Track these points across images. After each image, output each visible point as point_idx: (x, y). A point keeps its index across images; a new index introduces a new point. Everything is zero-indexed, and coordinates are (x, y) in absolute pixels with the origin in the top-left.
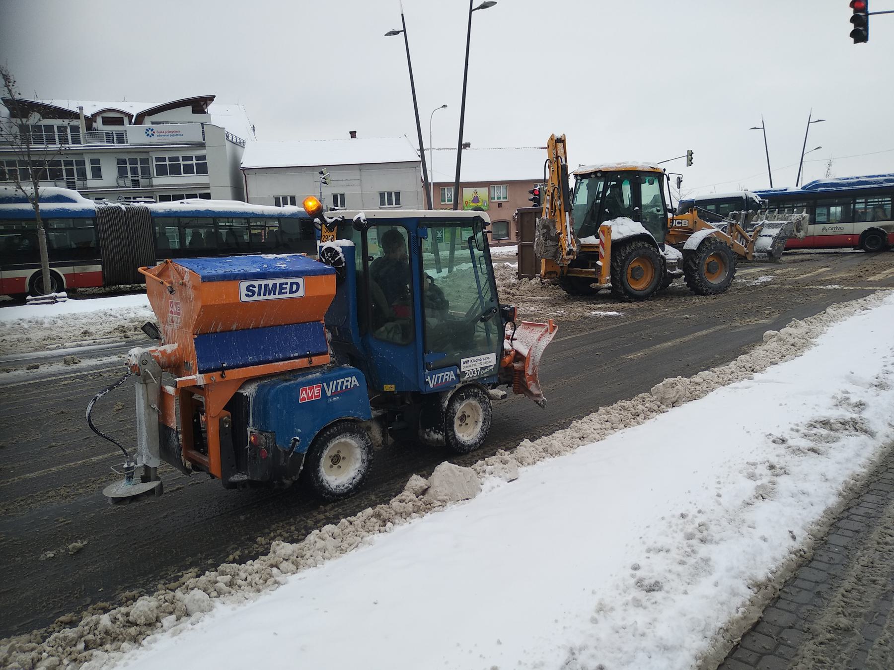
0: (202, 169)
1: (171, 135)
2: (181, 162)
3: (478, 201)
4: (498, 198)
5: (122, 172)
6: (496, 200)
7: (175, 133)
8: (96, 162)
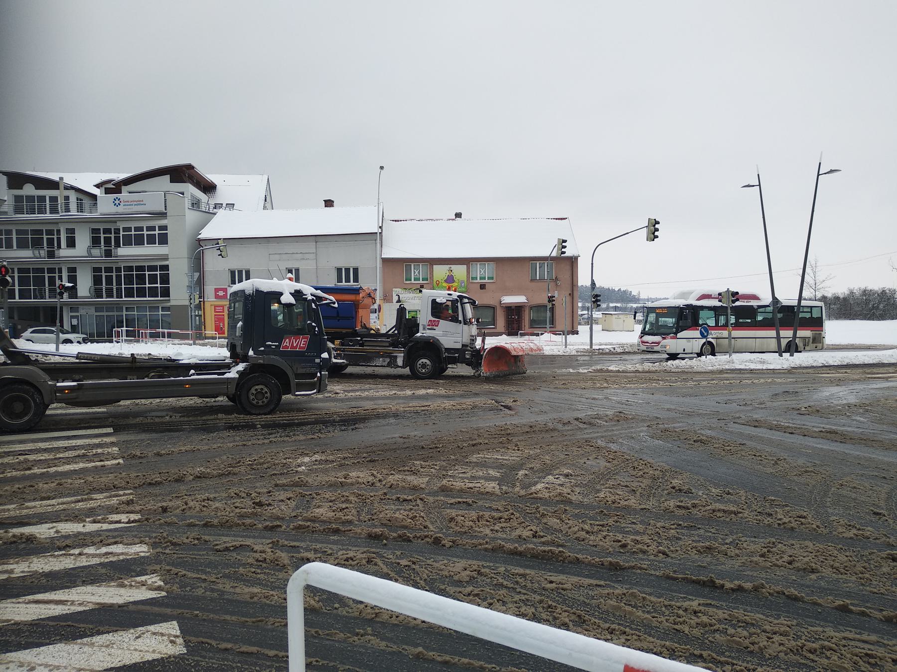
0: (163, 240)
1: (135, 205)
2: (145, 232)
3: (454, 281)
4: (481, 278)
5: (95, 242)
6: (478, 280)
7: (140, 203)
8: (71, 231)
